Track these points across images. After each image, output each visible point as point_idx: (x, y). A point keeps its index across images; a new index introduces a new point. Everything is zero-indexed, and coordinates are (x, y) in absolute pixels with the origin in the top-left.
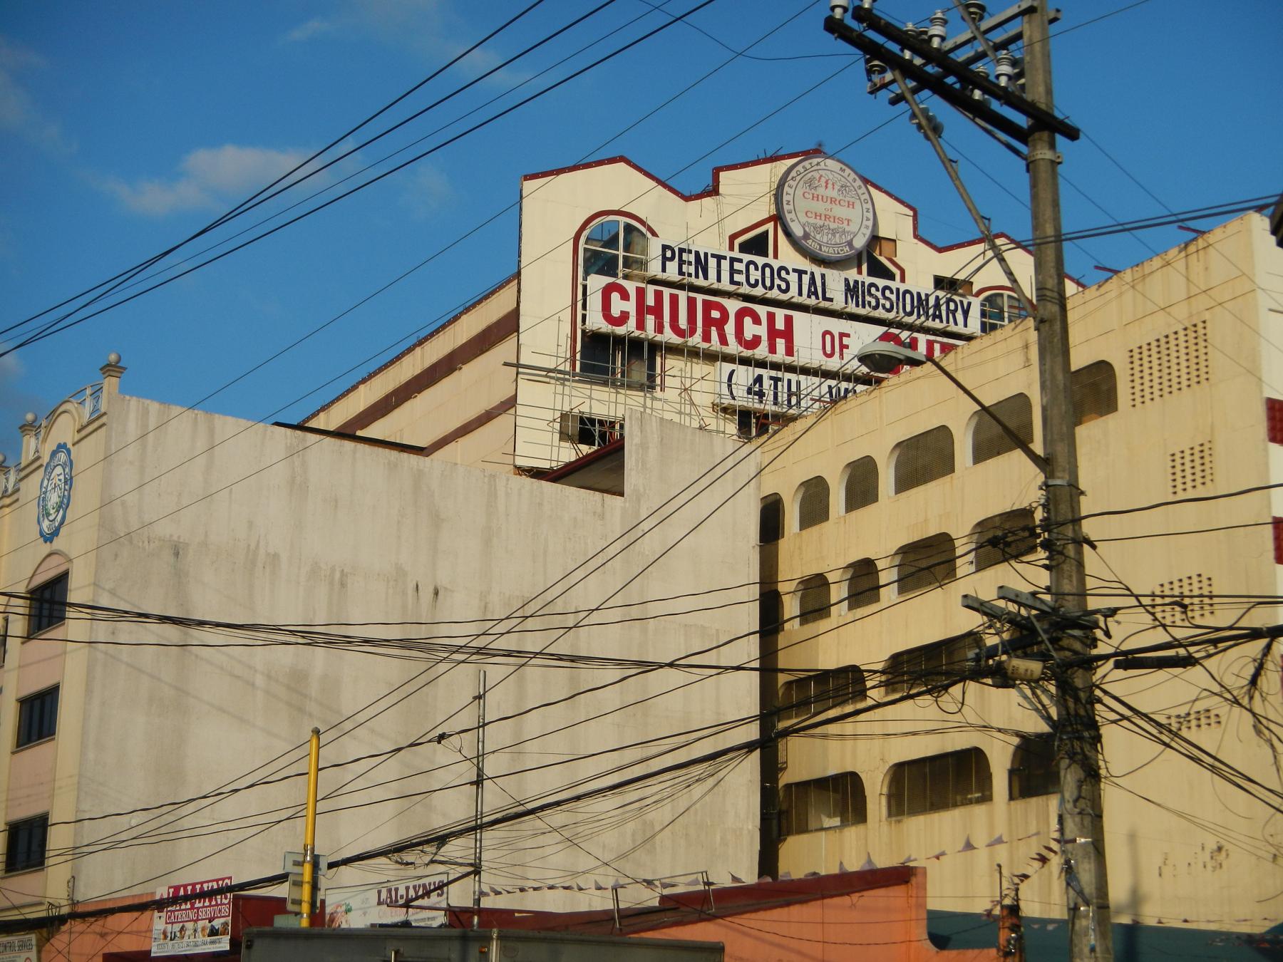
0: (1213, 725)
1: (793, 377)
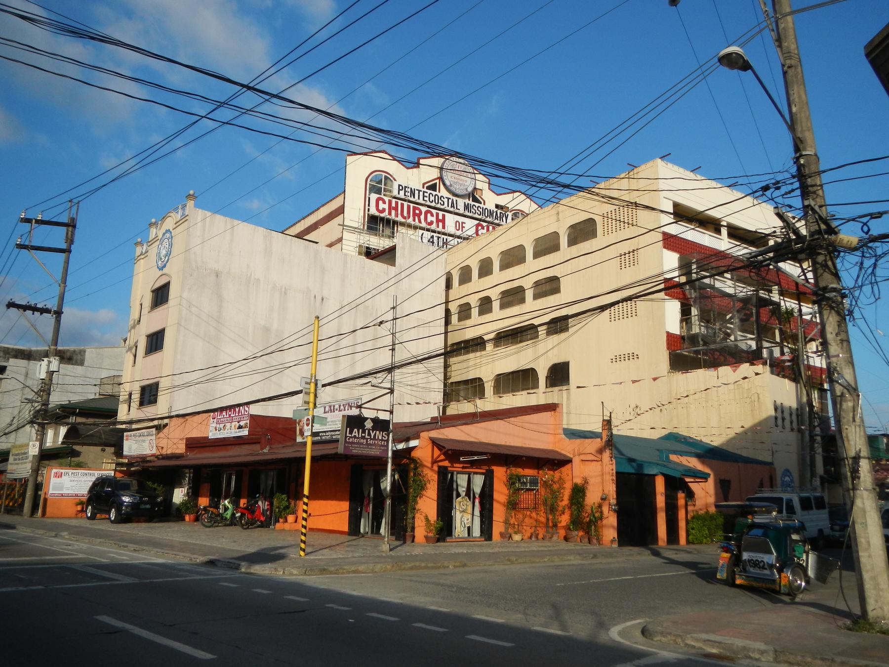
1: (445, 237)
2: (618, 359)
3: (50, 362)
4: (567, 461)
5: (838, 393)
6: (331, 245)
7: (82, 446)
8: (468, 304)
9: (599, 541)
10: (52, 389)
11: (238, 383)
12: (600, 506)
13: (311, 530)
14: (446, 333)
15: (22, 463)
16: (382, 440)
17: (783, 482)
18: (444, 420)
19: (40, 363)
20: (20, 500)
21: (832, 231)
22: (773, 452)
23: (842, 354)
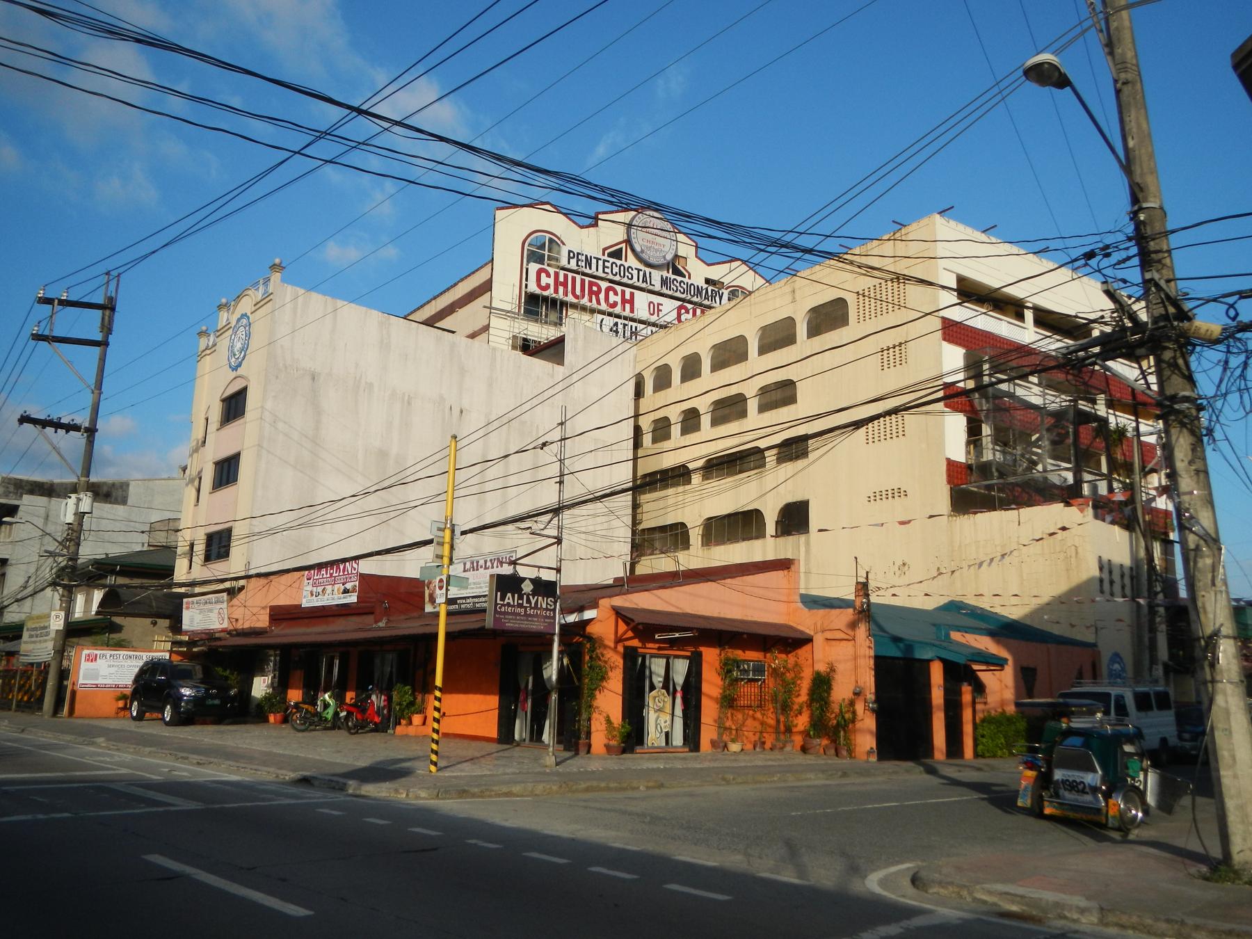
1: (634, 324)
2: (878, 497)
3: (79, 500)
5: (1192, 546)
6: (473, 336)
8: (666, 419)
9: (851, 752)
10: (82, 538)
11: (343, 529)
12: (852, 703)
14: (635, 459)
16: (547, 609)
18: (632, 582)
19: (66, 501)
20: (38, 693)
21: (1184, 316)
23: (1197, 490)
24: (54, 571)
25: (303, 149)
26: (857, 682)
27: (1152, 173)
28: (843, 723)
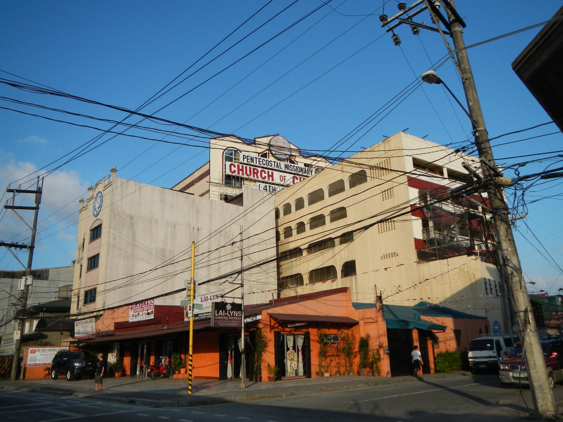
0: (396, 256)
1: (274, 186)
2: (386, 257)
3: (26, 279)
4: (355, 324)
5: (510, 272)
6: (202, 195)
7: (48, 332)
8: (290, 227)
9: (379, 373)
10: (28, 296)
11: (147, 285)
12: (378, 351)
13: (196, 377)
14: (277, 246)
15: (9, 345)
16: (238, 317)
17: (494, 329)
18: (279, 301)
19: (20, 280)
20: (9, 369)
21: (498, 175)
22: (486, 310)
23: (510, 248)
24: (15, 312)
25: (122, 121)
26: (380, 341)
27: (480, 116)
28: (375, 360)
